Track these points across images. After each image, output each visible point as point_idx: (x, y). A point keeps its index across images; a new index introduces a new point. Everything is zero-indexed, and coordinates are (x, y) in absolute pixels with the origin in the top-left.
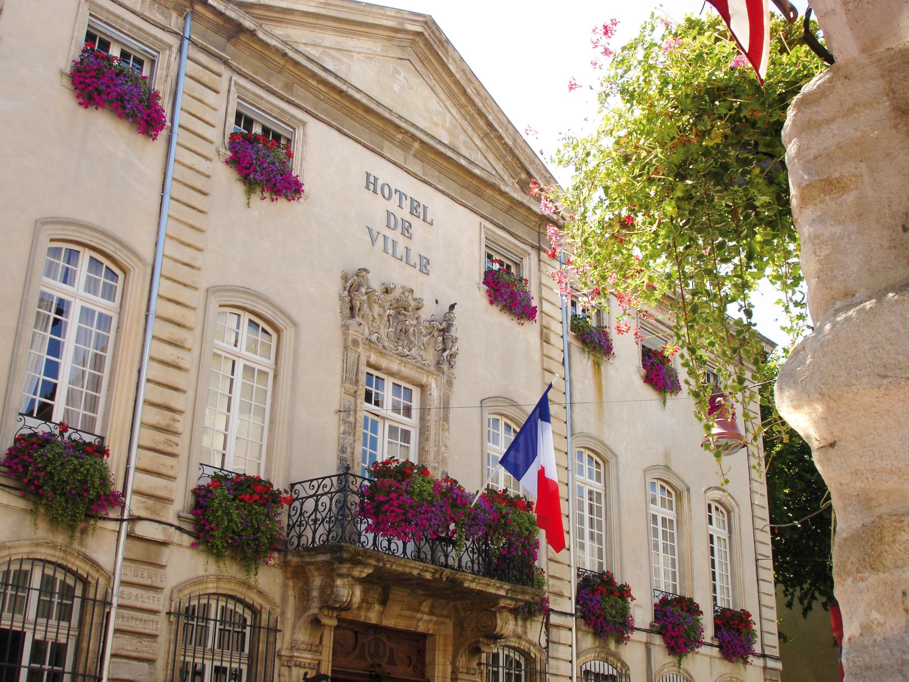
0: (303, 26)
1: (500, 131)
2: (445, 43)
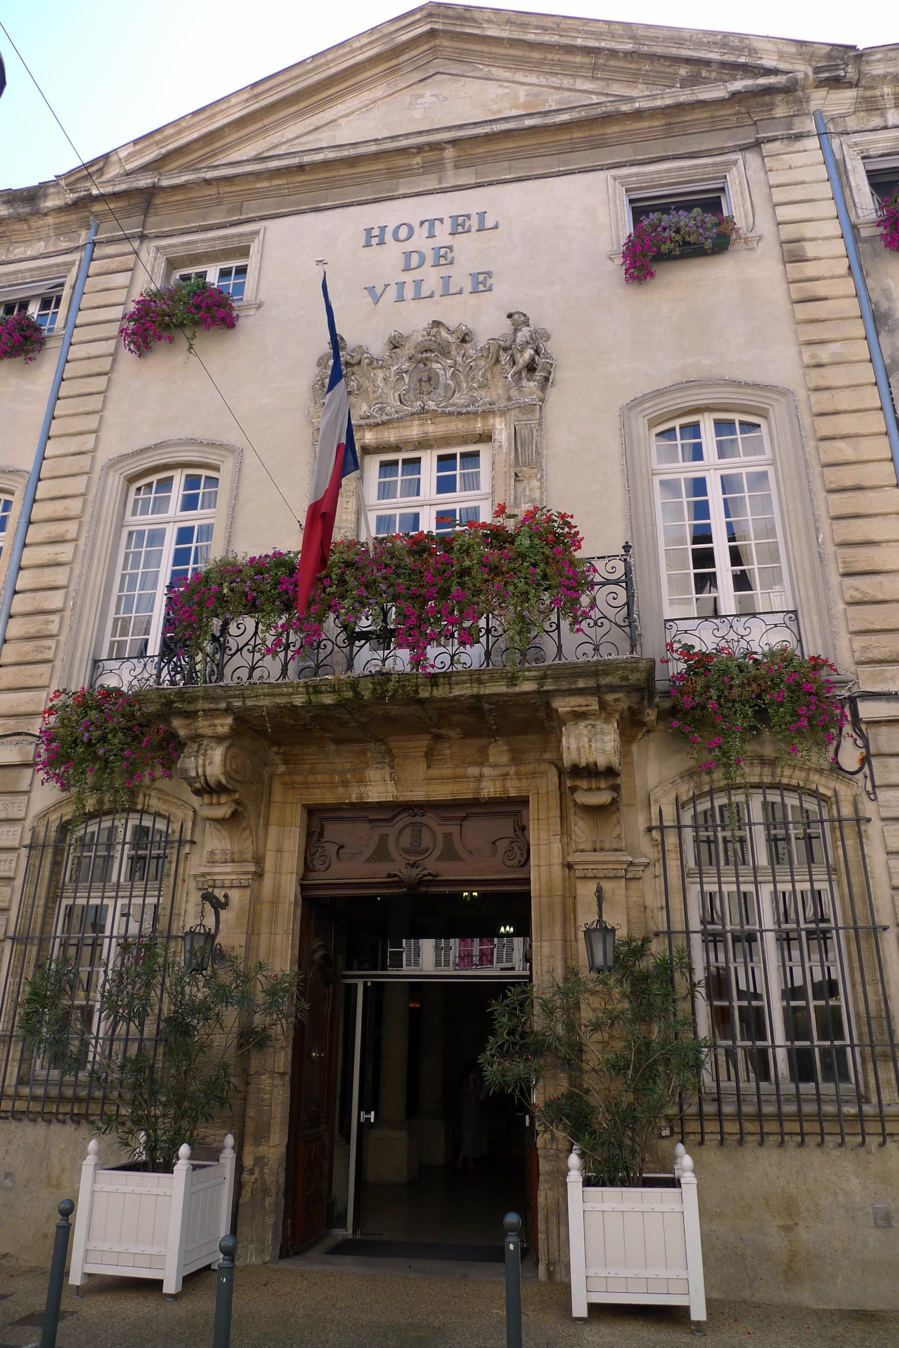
0: (248, 140)
1: (603, 44)
2: (466, 14)
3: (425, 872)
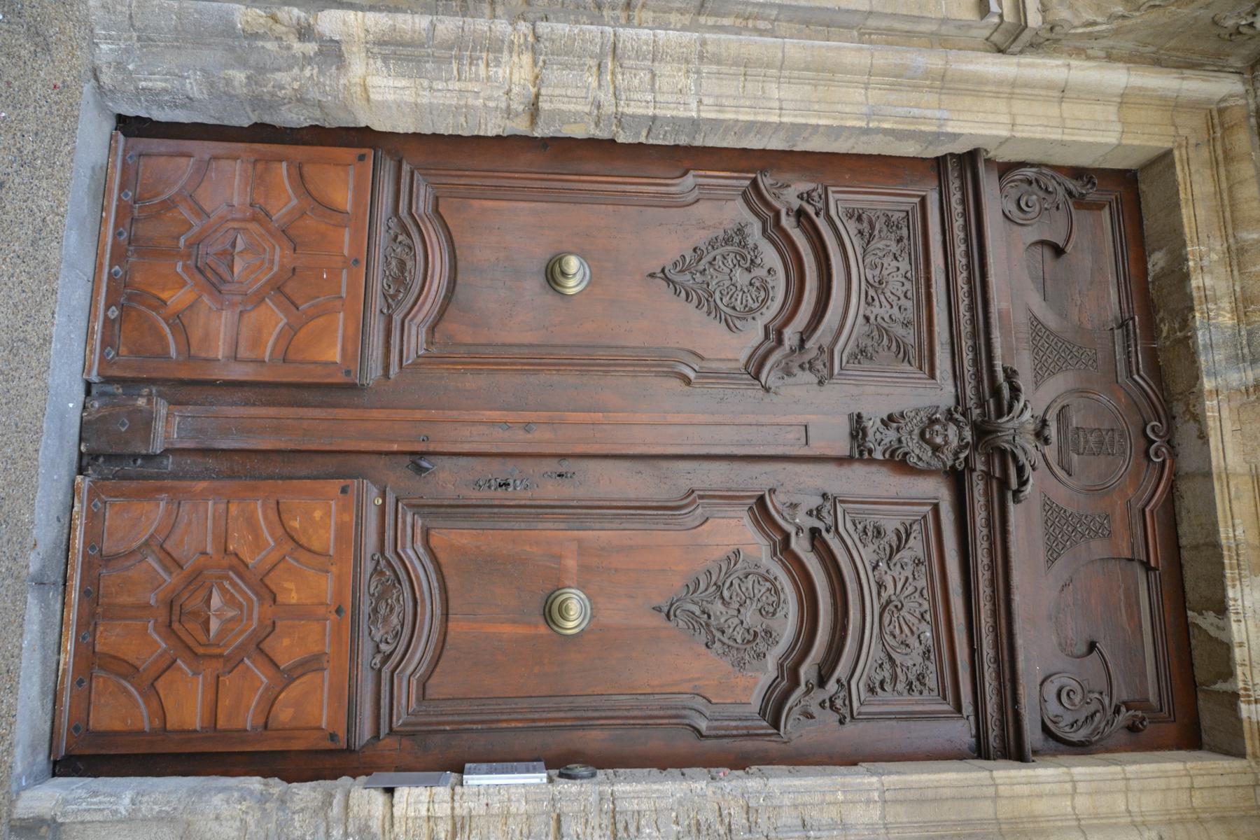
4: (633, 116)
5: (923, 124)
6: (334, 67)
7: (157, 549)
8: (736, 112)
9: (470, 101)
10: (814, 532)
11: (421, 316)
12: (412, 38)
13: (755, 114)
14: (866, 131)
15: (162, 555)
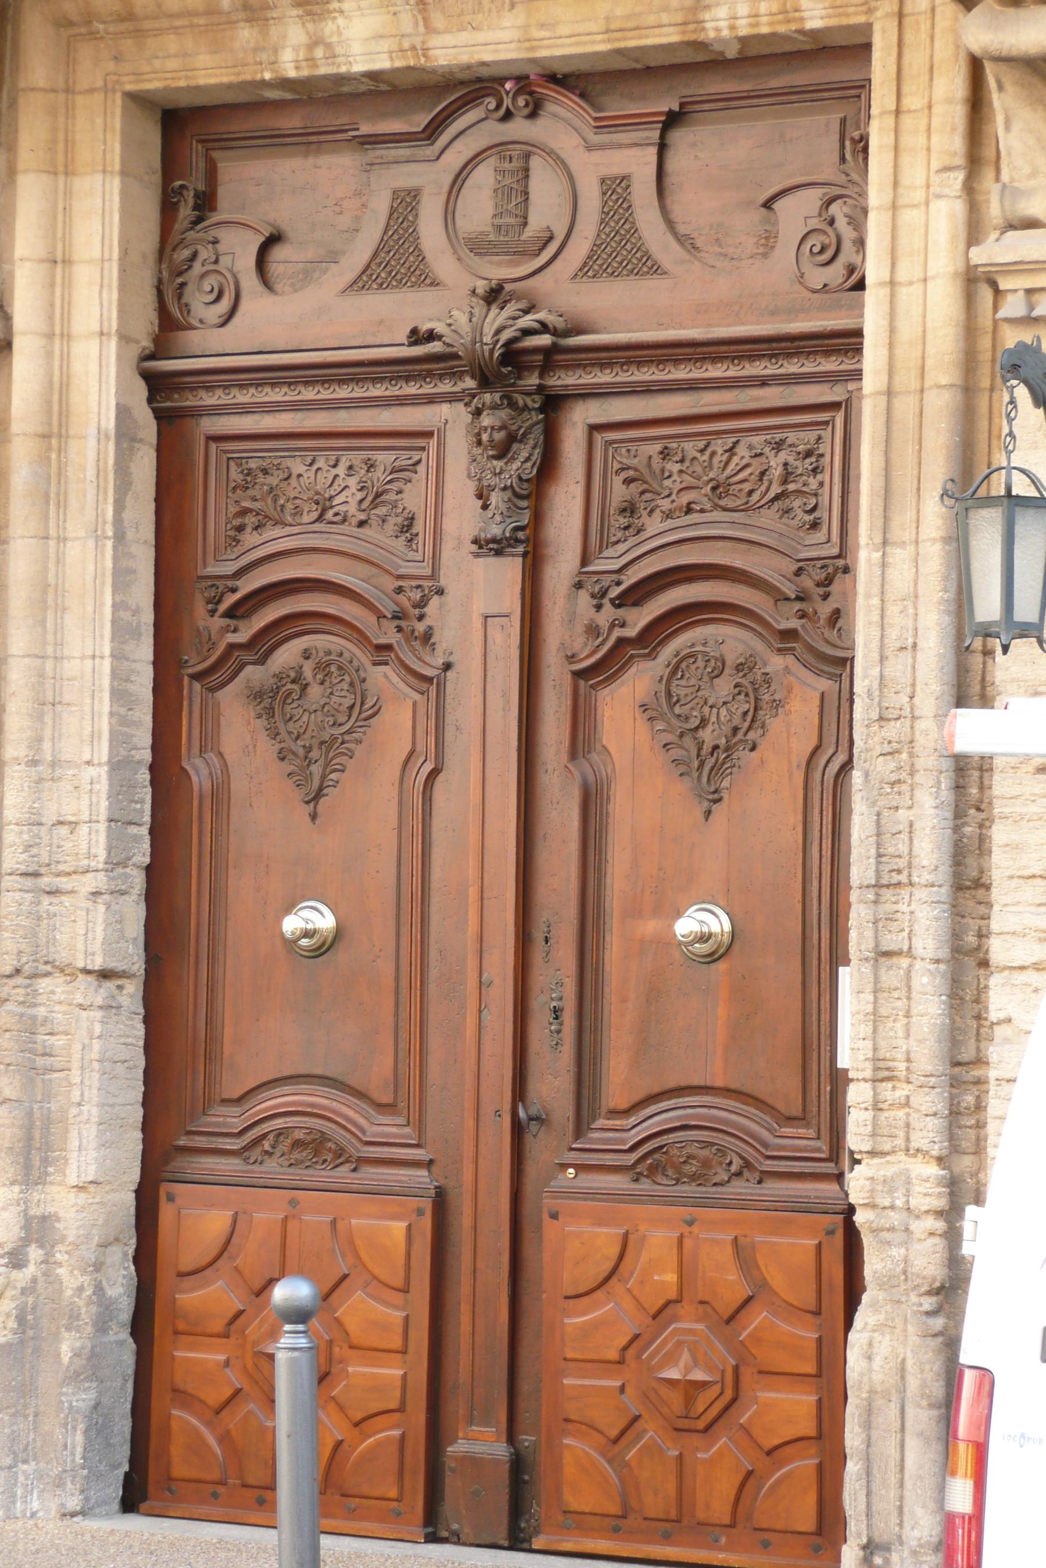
3: (527, 321)
4: (109, 850)
5: (106, 463)
6: (57, 1225)
7: (617, 1448)
8: (100, 716)
9: (95, 1055)
10: (620, 602)
11: (362, 1121)
12: (21, 1127)
13: (101, 691)
14: (119, 537)
15: (624, 1441)
